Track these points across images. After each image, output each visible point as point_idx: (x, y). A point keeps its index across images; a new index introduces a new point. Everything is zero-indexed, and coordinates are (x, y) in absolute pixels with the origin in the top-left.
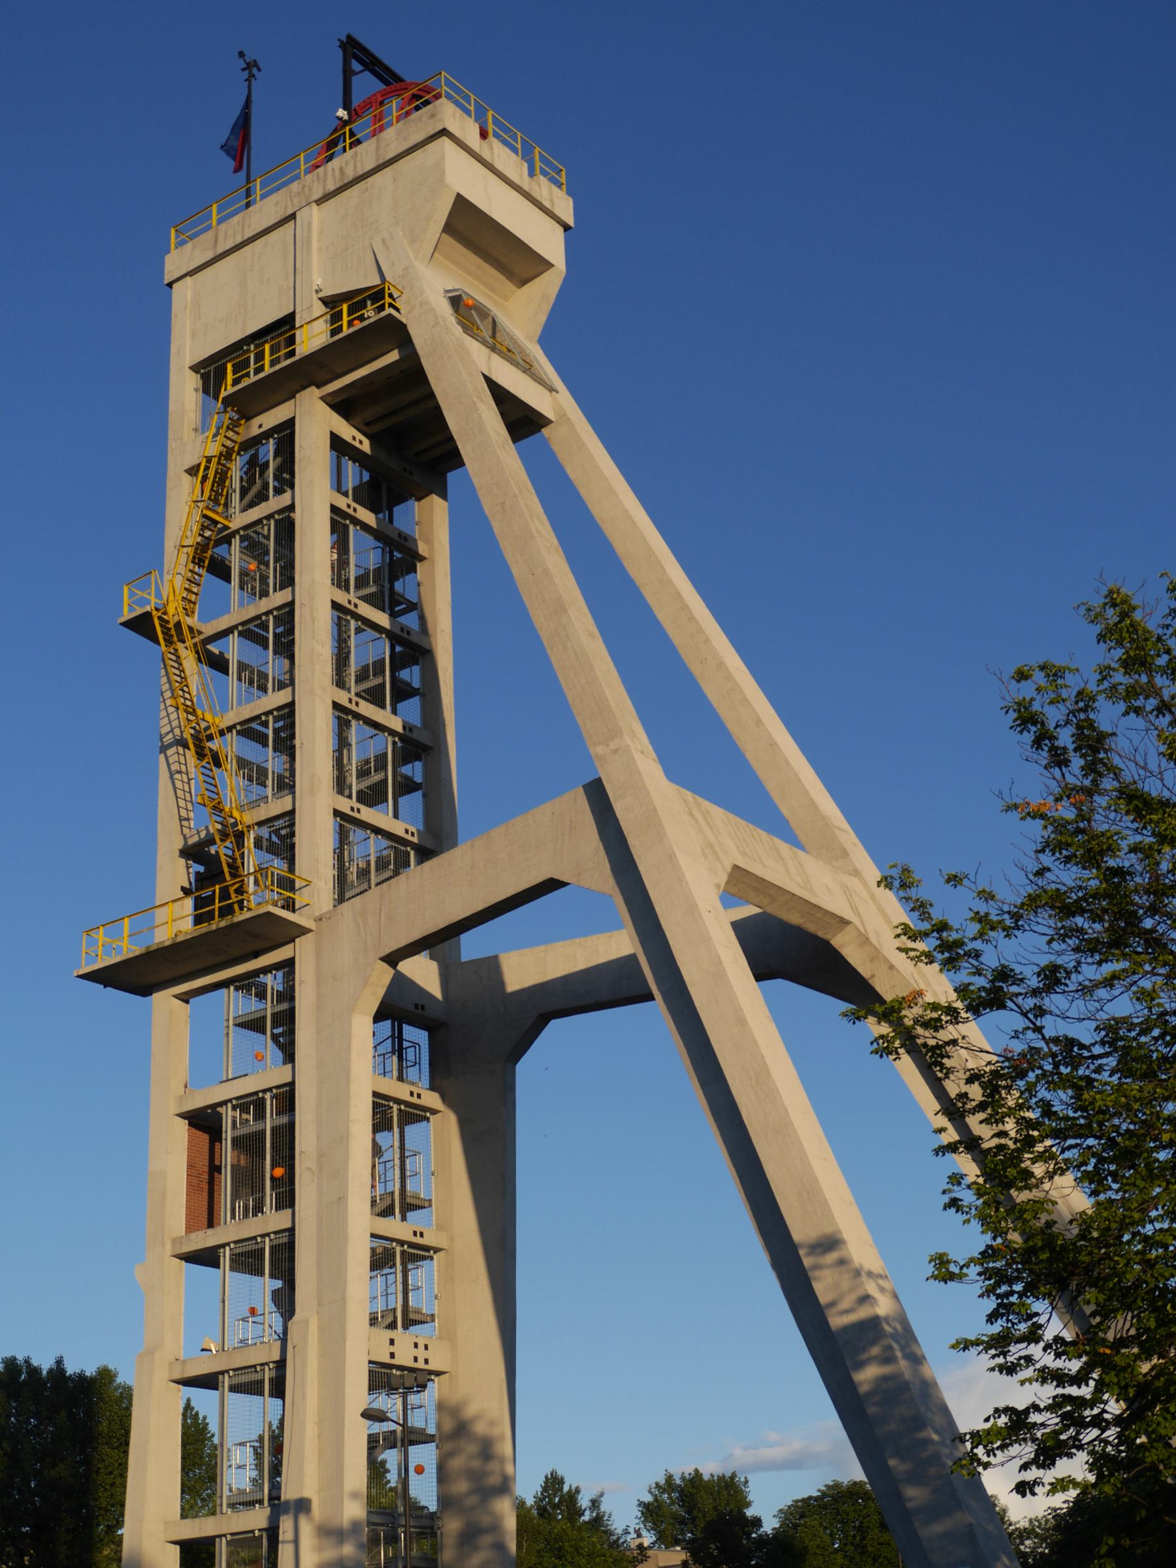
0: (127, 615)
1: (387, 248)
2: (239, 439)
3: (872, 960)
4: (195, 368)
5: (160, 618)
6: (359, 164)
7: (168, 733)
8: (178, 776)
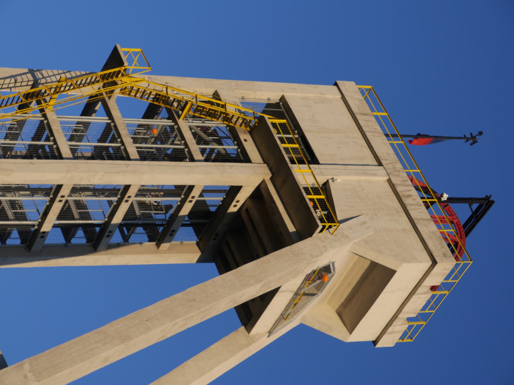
0: (121, 50)
1: (361, 225)
6: (413, 207)
7: (42, 75)
8: (13, 80)
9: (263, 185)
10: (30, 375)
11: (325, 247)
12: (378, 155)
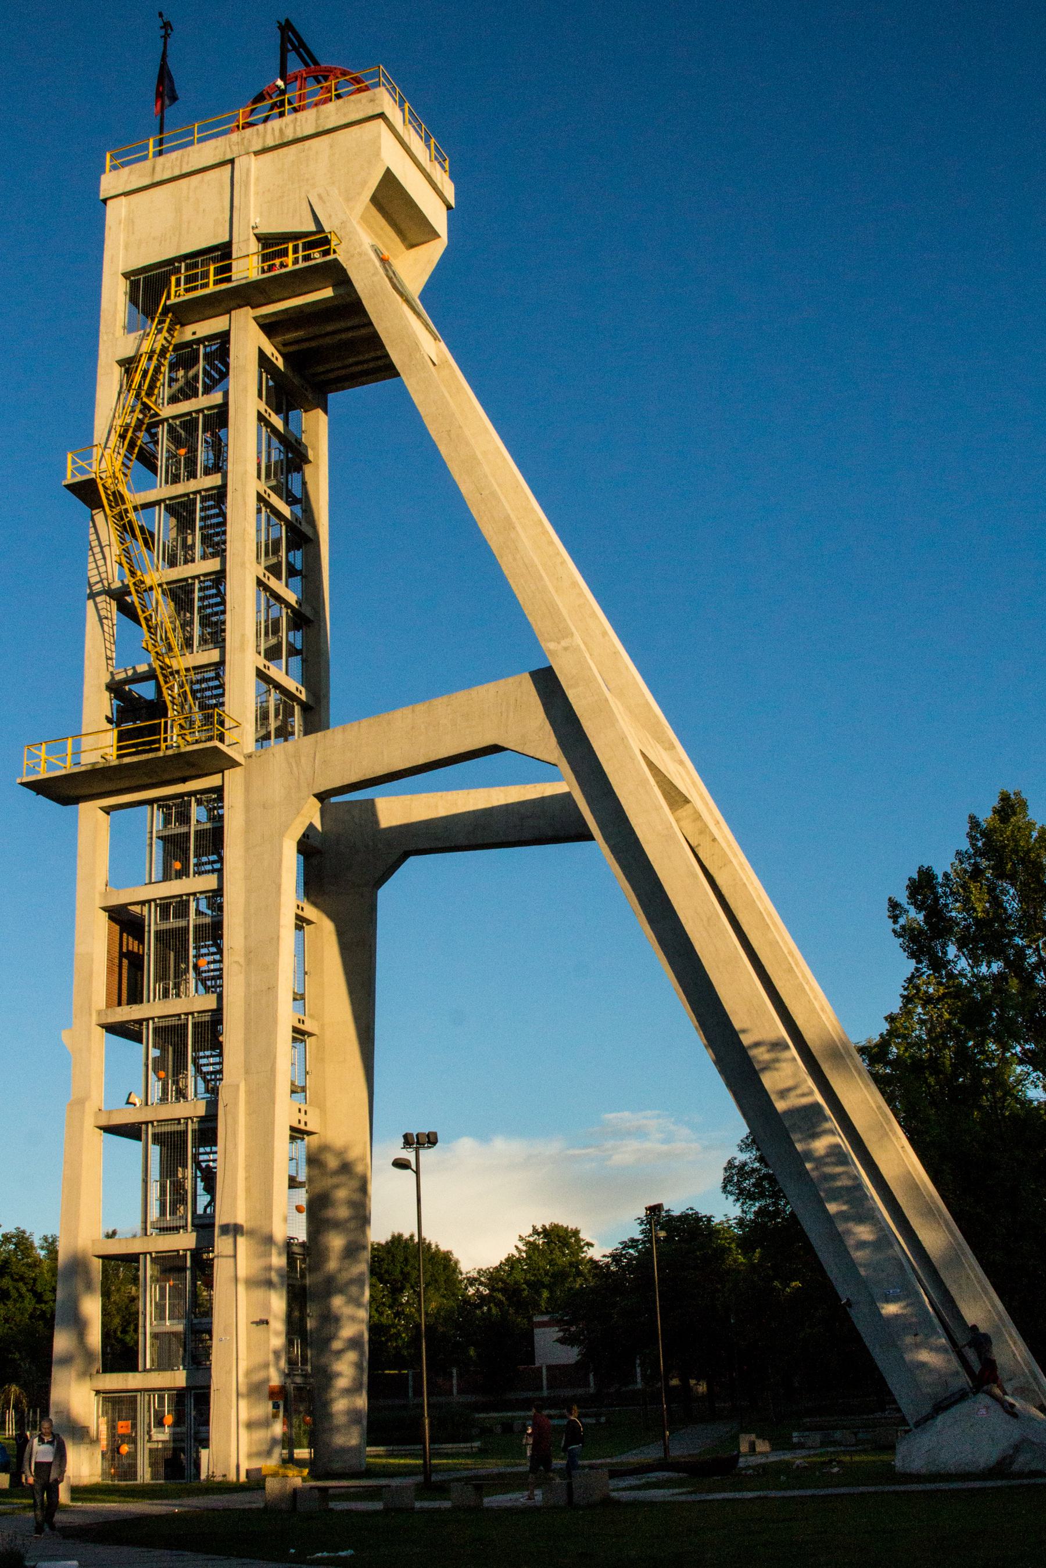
0: (69, 480)
1: (324, 202)
2: (173, 342)
3: (701, 833)
4: (126, 275)
5: (103, 485)
6: (298, 129)
7: (97, 583)
8: (105, 621)
9: (260, 320)
10: (564, 643)
11: (360, 254)
12: (217, 161)
